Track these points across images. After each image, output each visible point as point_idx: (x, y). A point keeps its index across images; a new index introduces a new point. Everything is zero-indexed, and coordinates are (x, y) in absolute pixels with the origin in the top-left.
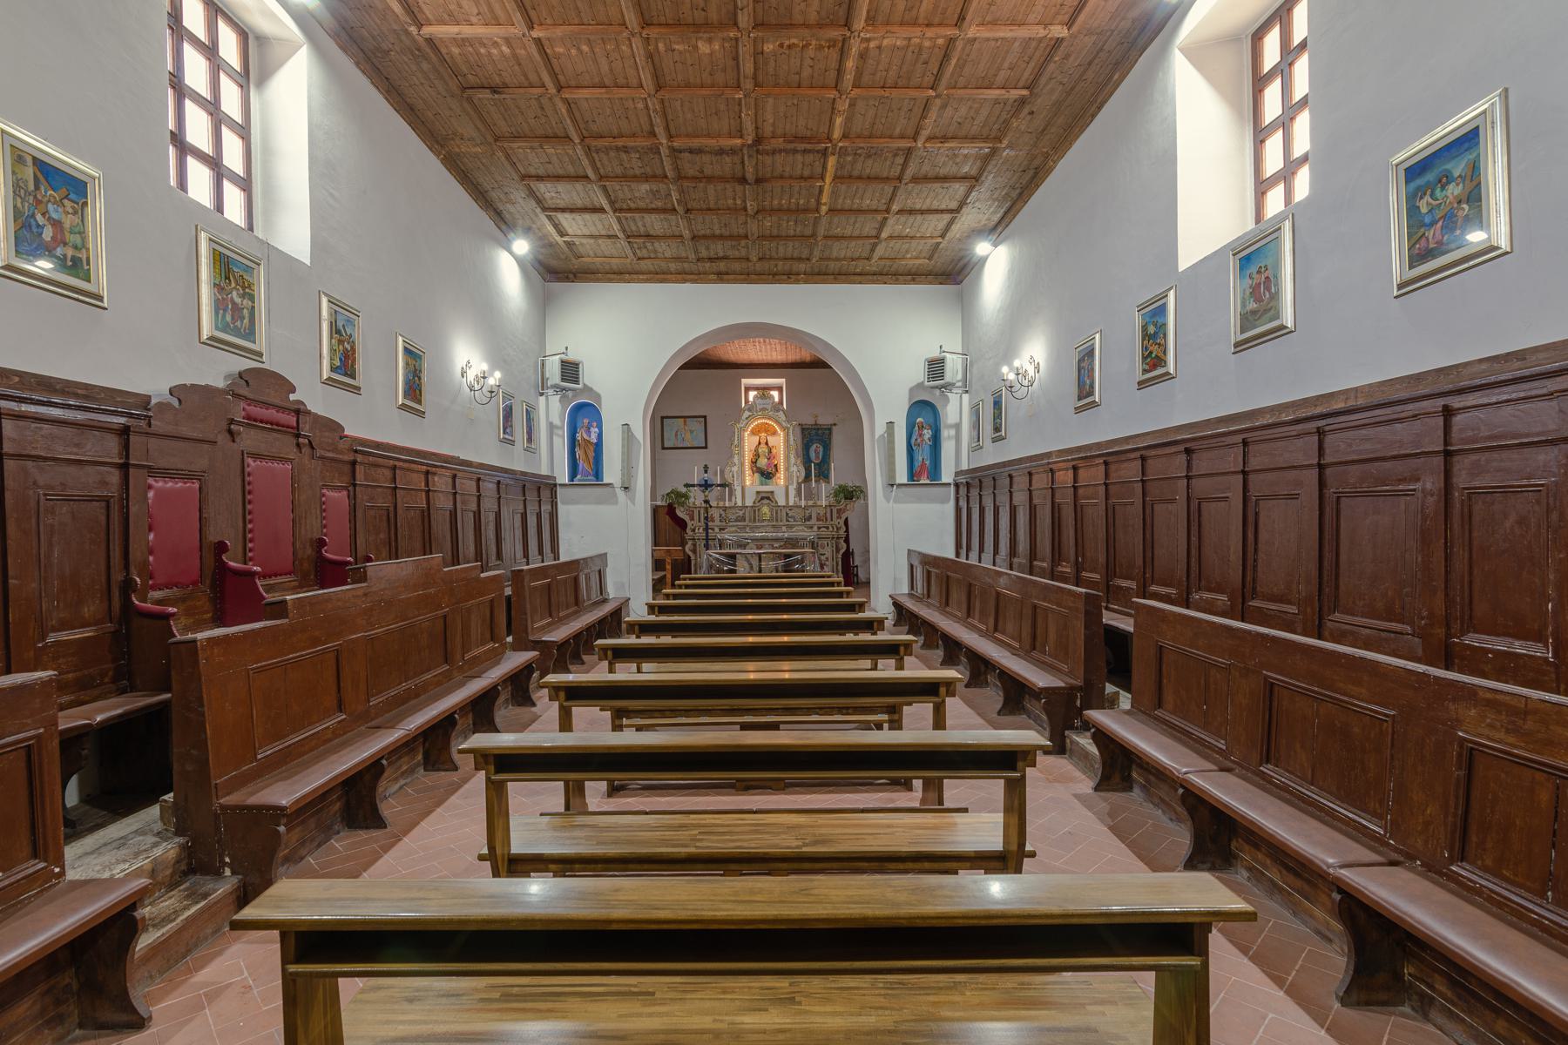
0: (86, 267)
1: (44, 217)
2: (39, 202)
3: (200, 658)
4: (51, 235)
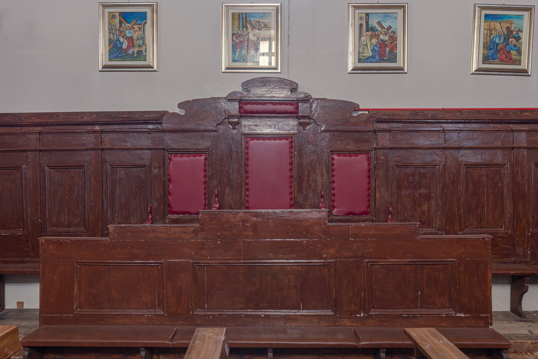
0: (145, 54)
1: (124, 38)
2: (121, 32)
3: (40, 249)
4: (127, 45)
